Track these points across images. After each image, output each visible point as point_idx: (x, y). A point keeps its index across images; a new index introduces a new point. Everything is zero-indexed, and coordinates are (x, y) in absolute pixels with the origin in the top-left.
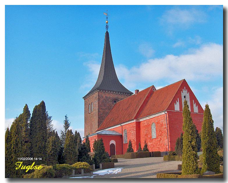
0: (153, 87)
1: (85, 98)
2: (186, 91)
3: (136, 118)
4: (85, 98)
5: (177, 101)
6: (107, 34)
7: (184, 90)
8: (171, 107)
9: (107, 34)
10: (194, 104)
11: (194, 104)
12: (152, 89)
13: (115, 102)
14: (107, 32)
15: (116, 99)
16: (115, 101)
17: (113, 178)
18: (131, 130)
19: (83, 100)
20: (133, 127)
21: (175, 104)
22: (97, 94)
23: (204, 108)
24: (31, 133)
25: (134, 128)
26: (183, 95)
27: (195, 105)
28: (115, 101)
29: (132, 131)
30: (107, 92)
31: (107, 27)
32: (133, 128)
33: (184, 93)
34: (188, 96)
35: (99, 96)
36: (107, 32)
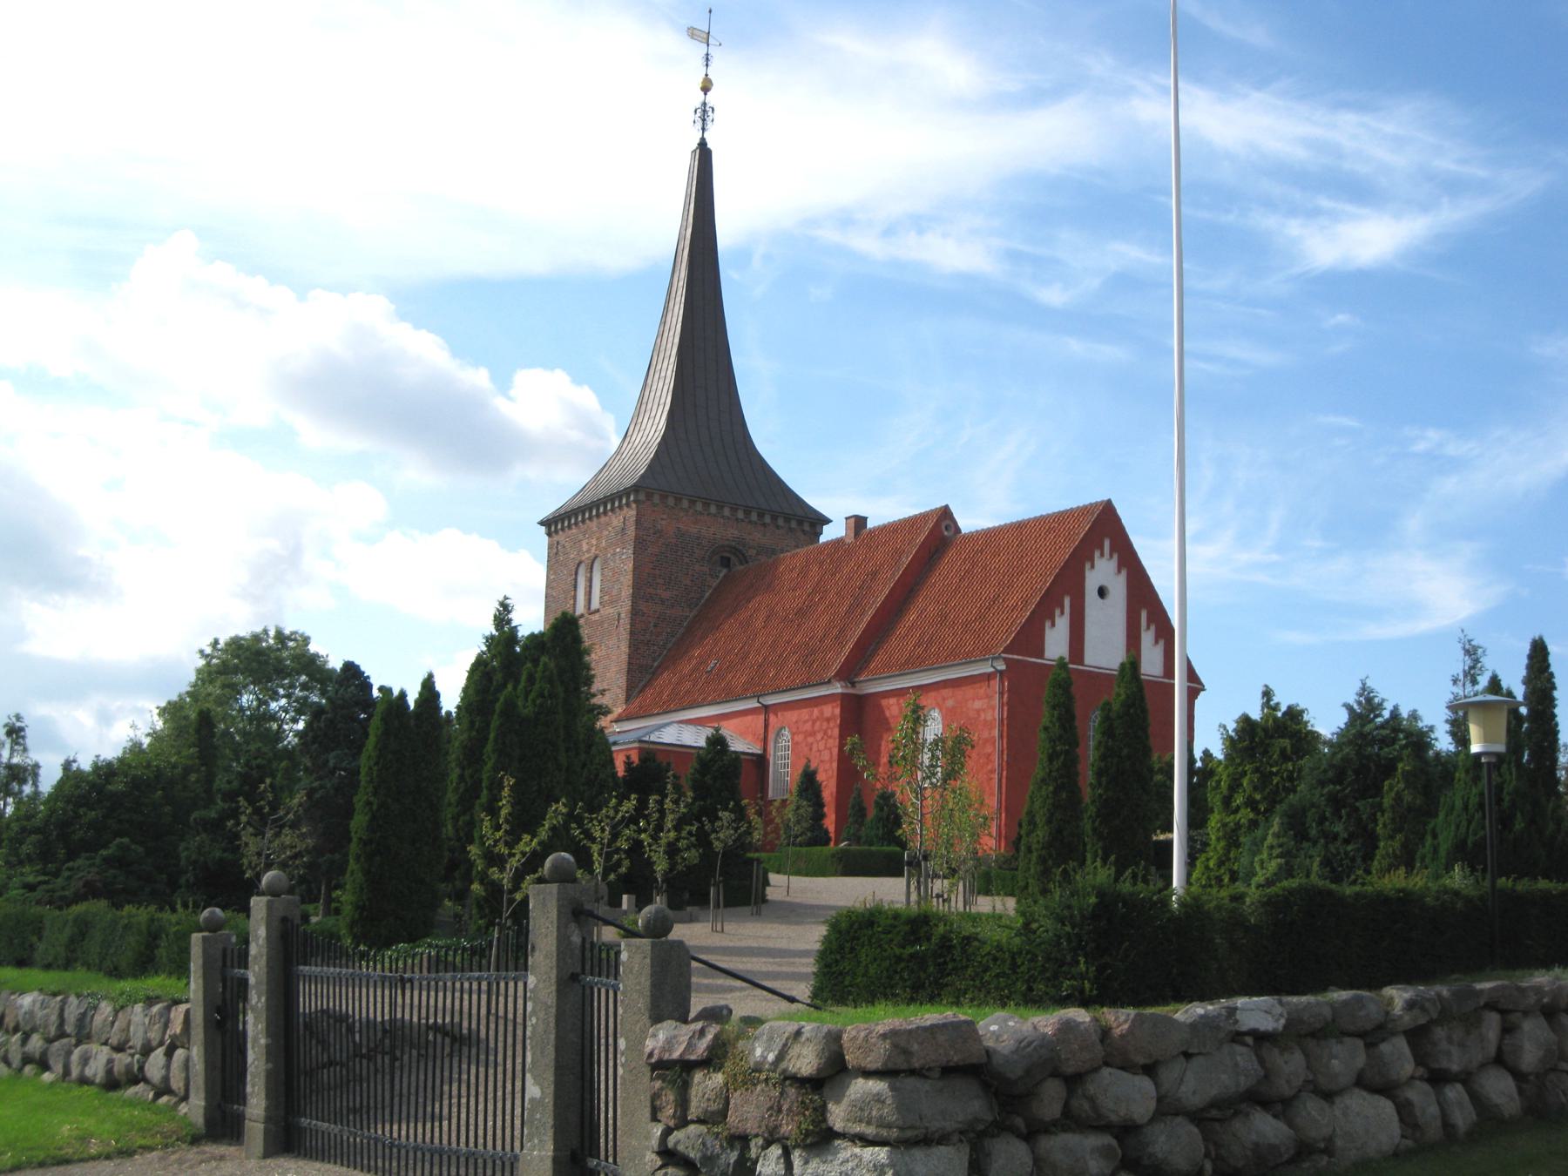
0: (945, 514)
1: (552, 524)
2: (1113, 564)
3: (848, 673)
4: (552, 524)
5: (1062, 613)
6: (704, 155)
7: (1102, 555)
8: (1030, 638)
9: (704, 155)
10: (1148, 628)
11: (1148, 628)
12: (937, 524)
13: (726, 562)
14: (703, 145)
15: (736, 551)
16: (729, 559)
17: (528, 1047)
18: (813, 734)
19: (541, 537)
20: (828, 720)
21: (1048, 624)
22: (631, 513)
23: (1161, 643)
24: (593, 710)
25: (832, 725)
26: (1093, 580)
27: (1147, 637)
28: (729, 559)
29: (819, 736)
30: (685, 504)
31: (704, 113)
32: (825, 724)
33: (1103, 571)
34: (1118, 587)
35: (638, 522)
36: (703, 145)
